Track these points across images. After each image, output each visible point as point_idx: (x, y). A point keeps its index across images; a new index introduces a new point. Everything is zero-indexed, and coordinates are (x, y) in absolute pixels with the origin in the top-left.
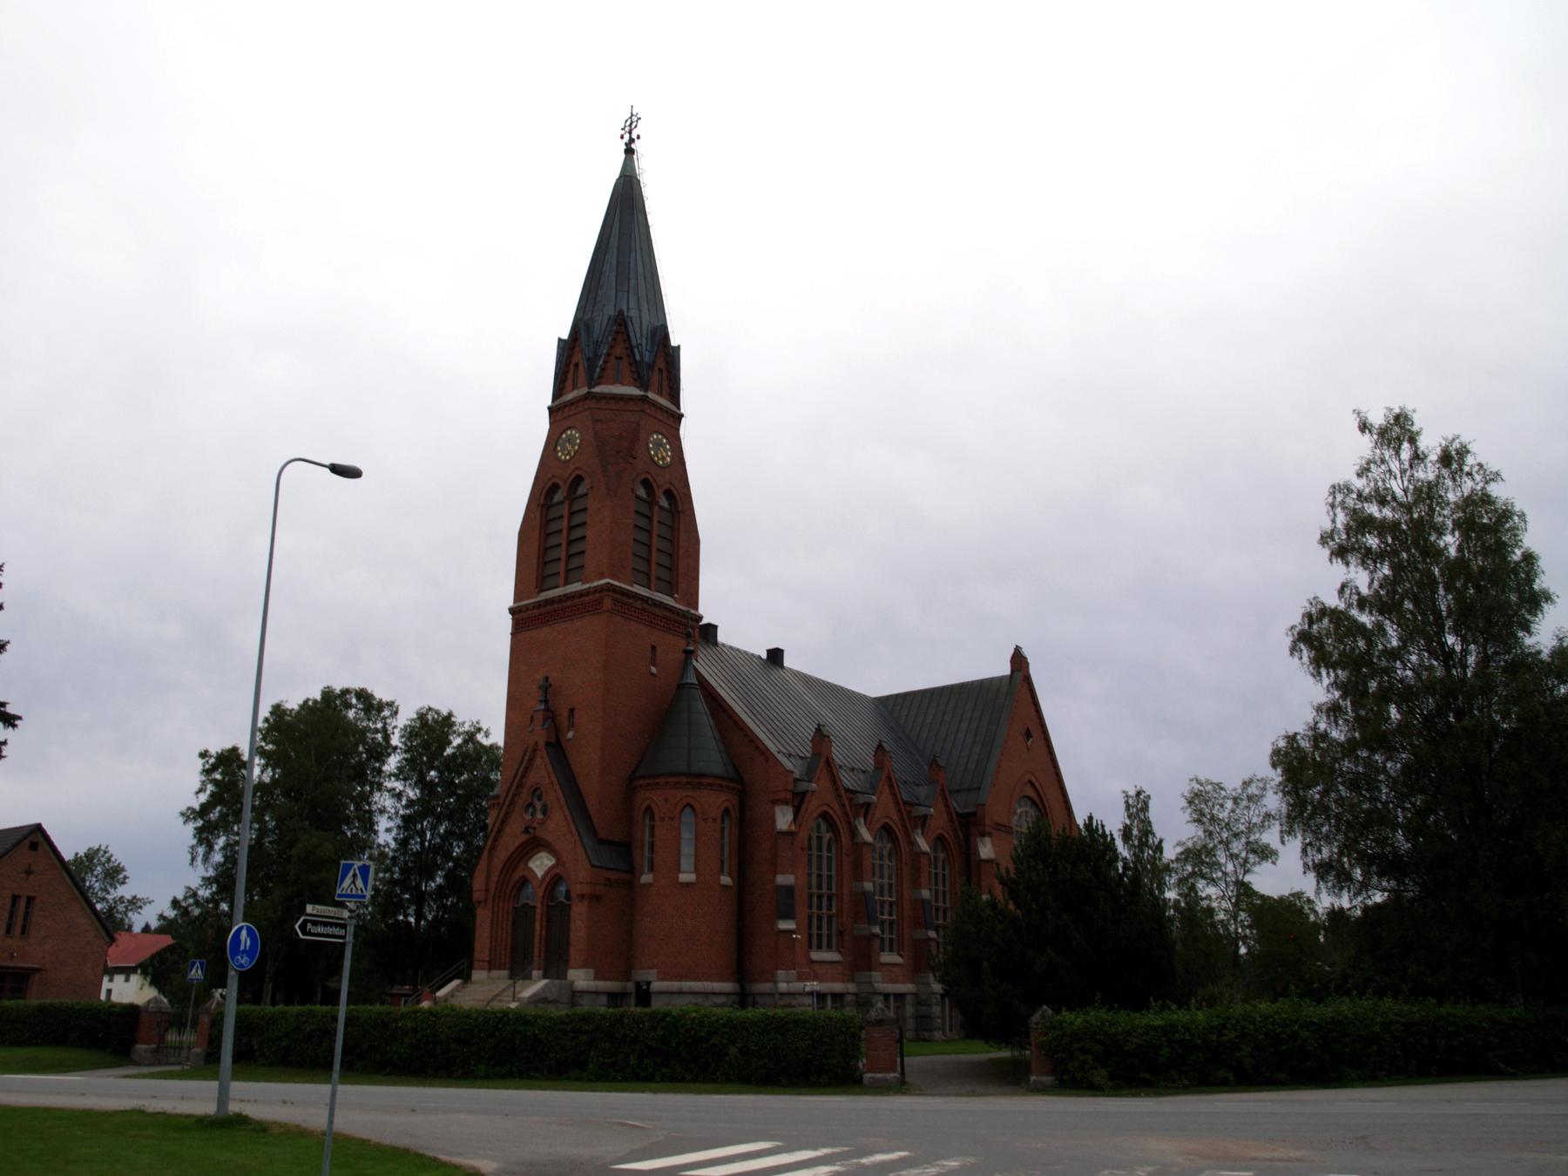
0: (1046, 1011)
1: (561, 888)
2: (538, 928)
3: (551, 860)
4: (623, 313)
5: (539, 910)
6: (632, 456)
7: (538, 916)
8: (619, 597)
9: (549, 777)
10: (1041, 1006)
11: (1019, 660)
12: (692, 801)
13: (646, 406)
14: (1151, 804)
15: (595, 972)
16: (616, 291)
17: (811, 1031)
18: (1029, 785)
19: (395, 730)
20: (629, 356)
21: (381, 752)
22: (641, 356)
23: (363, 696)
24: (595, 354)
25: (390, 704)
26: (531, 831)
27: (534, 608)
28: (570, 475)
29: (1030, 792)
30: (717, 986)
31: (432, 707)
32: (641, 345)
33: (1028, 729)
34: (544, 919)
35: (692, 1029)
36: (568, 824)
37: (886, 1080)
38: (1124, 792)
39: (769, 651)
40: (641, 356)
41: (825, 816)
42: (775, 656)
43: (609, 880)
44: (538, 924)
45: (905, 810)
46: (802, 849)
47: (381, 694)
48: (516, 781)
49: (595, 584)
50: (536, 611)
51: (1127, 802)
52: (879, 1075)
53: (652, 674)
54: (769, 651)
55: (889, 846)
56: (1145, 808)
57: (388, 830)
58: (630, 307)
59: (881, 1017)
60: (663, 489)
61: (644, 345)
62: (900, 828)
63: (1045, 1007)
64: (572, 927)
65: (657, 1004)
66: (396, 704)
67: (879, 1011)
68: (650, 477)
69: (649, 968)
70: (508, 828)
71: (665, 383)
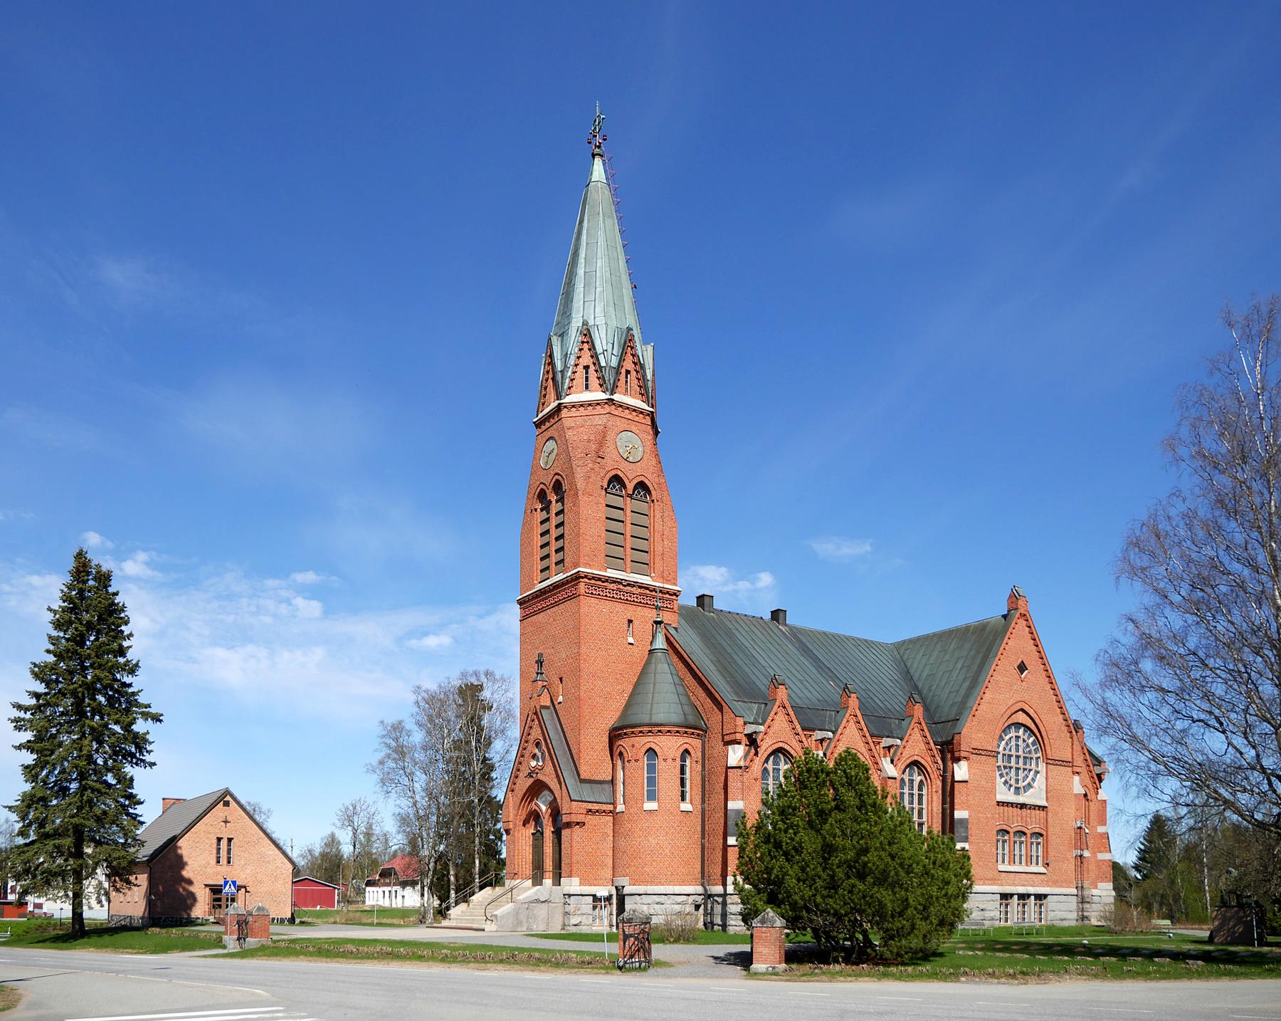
8: (593, 581)
11: (1014, 598)
12: (653, 746)
15: (580, 879)
20: (594, 364)
24: (566, 366)
26: (534, 775)
35: (830, 856)
42: (777, 615)
43: (590, 810)
45: (873, 742)
46: (756, 780)
49: (571, 573)
68: (619, 473)
69: (624, 876)
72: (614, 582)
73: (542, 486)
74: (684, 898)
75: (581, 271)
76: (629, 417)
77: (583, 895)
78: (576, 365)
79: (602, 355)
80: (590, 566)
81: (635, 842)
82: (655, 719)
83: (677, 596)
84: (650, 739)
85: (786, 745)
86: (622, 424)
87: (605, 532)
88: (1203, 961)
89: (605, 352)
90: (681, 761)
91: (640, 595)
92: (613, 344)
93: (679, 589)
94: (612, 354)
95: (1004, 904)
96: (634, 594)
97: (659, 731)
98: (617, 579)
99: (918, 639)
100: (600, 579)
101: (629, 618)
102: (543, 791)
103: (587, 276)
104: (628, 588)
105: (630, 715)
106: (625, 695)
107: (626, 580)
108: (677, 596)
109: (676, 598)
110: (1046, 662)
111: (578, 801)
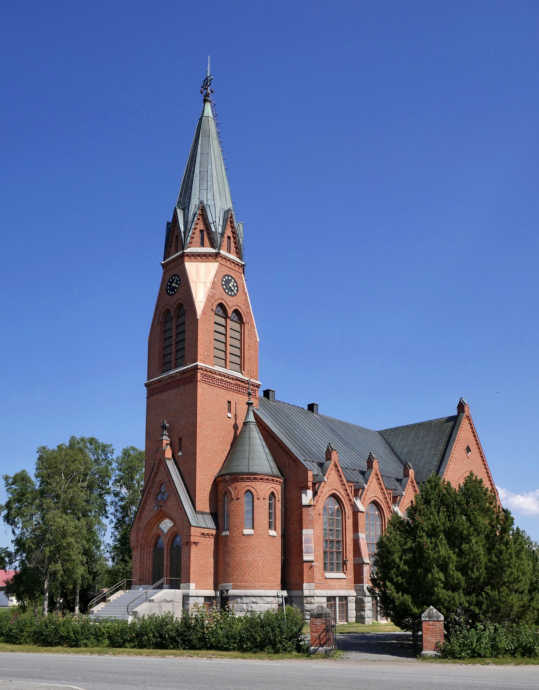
0: (432, 610)
1: (178, 539)
2: (165, 561)
7: (165, 555)
10: (429, 606)
11: (461, 407)
12: (251, 489)
16: (200, 190)
21: (104, 475)
22: (216, 229)
23: (92, 441)
30: (274, 592)
33: (468, 446)
34: (169, 556)
40: (216, 229)
41: (334, 496)
42: (311, 407)
43: (203, 534)
44: (165, 559)
45: (387, 493)
47: (102, 440)
48: (150, 480)
50: (159, 384)
58: (208, 199)
59: (320, 612)
61: (217, 222)
62: (384, 503)
63: (431, 607)
64: (182, 561)
66: (113, 447)
68: (223, 302)
70: (147, 507)
71: (233, 245)
73: (166, 307)
74: (272, 599)
76: (230, 266)
77: (197, 597)
78: (195, 229)
79: (213, 224)
80: (204, 362)
81: (237, 558)
83: (258, 388)
84: (248, 484)
85: (337, 492)
87: (213, 340)
89: (215, 223)
90: (269, 501)
91: (236, 385)
92: (219, 218)
93: (260, 383)
94: (219, 224)
95: (341, 616)
96: (231, 384)
99: (397, 429)
102: (165, 519)
103: (201, 174)
105: (233, 466)
108: (258, 388)
109: (258, 389)
110: (480, 447)
111: (195, 527)
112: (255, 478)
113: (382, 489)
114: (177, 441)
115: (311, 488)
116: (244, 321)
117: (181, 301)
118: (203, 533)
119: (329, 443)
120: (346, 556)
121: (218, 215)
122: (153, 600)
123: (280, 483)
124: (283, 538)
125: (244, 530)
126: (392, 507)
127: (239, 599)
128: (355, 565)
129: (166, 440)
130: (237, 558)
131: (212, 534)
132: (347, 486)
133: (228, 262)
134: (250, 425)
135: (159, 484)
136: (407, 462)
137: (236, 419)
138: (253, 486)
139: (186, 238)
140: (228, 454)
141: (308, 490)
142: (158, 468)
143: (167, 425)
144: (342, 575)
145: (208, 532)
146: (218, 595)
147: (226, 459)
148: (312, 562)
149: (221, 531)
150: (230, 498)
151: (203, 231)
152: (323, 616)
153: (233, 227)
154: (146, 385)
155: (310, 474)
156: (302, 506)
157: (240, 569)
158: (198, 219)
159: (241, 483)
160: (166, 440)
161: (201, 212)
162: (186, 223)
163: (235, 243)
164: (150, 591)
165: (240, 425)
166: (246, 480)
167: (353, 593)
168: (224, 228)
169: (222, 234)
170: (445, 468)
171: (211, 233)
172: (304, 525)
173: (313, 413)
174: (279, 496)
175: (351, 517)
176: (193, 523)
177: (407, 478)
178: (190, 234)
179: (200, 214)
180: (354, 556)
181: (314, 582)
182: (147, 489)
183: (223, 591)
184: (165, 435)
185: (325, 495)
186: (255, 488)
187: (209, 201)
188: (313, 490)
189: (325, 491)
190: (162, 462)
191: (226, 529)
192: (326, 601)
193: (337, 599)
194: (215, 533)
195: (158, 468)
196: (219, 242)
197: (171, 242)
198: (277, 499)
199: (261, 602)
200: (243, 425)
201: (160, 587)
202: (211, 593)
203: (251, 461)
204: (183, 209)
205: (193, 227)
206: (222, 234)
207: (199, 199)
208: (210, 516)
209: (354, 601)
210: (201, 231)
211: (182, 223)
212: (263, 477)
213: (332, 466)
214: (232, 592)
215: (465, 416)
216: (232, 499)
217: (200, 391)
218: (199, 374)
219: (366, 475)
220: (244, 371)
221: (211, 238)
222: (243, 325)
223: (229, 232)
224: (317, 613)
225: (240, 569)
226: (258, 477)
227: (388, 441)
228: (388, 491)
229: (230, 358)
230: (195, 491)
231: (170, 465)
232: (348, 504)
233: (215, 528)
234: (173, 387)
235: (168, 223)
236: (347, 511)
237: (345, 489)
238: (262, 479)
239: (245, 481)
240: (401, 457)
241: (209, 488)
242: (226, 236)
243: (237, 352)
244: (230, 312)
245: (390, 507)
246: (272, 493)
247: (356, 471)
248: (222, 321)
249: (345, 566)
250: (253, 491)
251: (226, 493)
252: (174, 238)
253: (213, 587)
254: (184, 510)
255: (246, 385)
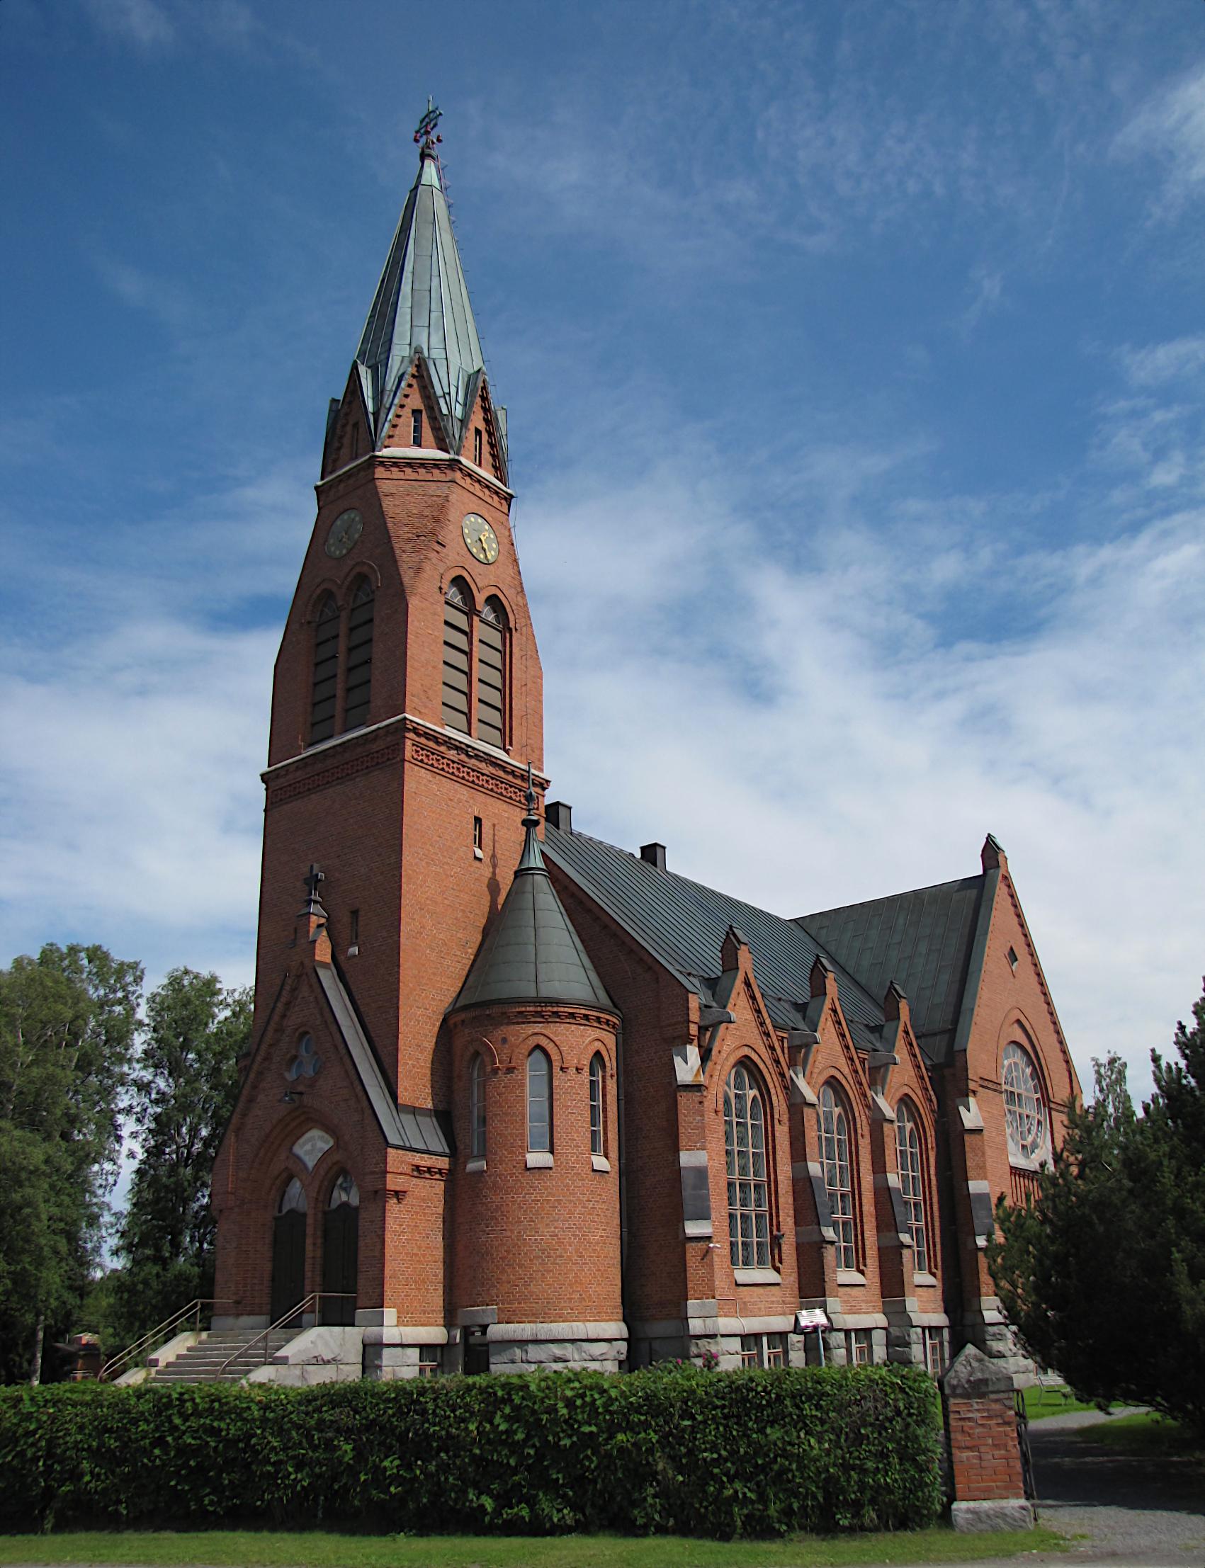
3: (327, 1142)
4: (422, 353)
5: (310, 1221)
6: (438, 543)
7: (309, 1230)
8: (423, 740)
9: (322, 1014)
11: (991, 852)
12: (544, 1042)
13: (458, 475)
14: (1128, 1073)
15: (398, 1312)
17: (832, 1414)
18: (1016, 1026)
19: (139, 1000)
21: (118, 1035)
22: (450, 410)
23: (97, 955)
25: (134, 966)
27: (297, 769)
28: (348, 575)
29: (1020, 1037)
31: (189, 968)
32: (449, 394)
34: (319, 1233)
36: (352, 1084)
37: (1002, 1515)
38: (1093, 1059)
39: (643, 849)
40: (450, 410)
42: (652, 853)
43: (417, 1168)
44: (309, 1241)
45: (859, 1058)
47: (119, 954)
50: (299, 773)
51: (1098, 1072)
52: (986, 1505)
53: (476, 858)
54: (643, 849)
55: (837, 1110)
56: (1121, 1078)
57: (134, 1135)
59: (979, 1375)
60: (486, 594)
62: (852, 1082)
64: (361, 1244)
65: (500, 1368)
66: (141, 966)
67: (975, 1364)
68: (465, 575)
71: (486, 449)
72: (457, 748)
75: (406, 288)
76: (480, 494)
78: (402, 406)
80: (421, 714)
82: (548, 990)
84: (538, 1028)
86: (474, 504)
88: (1069, 1381)
94: (457, 401)
97: (556, 1014)
98: (461, 742)
100: (436, 740)
101: (476, 814)
102: (310, 1129)
104: (473, 761)
106: (470, 951)
107: (474, 749)
108: (544, 789)
112: (556, 1014)
113: (847, 1047)
114: (346, 919)
115: (696, 1042)
116: (512, 625)
117: (365, 569)
118: (418, 1167)
119: (731, 926)
120: (778, 1223)
121: (453, 382)
122: (286, 1358)
123: (614, 1027)
124: (624, 1179)
125: (528, 1156)
126: (870, 1093)
127: (518, 1351)
128: (799, 1248)
129: (317, 916)
130: (508, 1233)
131: (440, 1169)
132: (774, 1038)
133: (477, 485)
134: (535, 877)
135: (297, 1034)
136: (892, 982)
137: (494, 866)
138: (551, 1036)
139: (380, 425)
140: (477, 956)
141: (688, 1047)
142: (294, 990)
143: (321, 875)
144: (769, 1276)
145: (429, 1164)
146: (458, 1340)
147: (472, 966)
148: (709, 1238)
149: (462, 1160)
150: (489, 1069)
151: (420, 411)
152: (991, 1388)
153: (486, 410)
154: (264, 777)
155: (694, 1003)
156: (675, 1089)
157: (520, 1266)
158: (410, 386)
159: (517, 1027)
160: (317, 916)
161: (417, 371)
162: (379, 393)
163: (492, 446)
164: (277, 1334)
165: (506, 879)
166: (533, 1020)
167: (879, 1319)
168: (467, 407)
169: (464, 422)
170: (974, 999)
171: (439, 417)
172: (683, 1141)
173: (655, 865)
174: (611, 1064)
175: (785, 1118)
176: (393, 1138)
177: (896, 1022)
178: (390, 417)
179: (413, 376)
180: (796, 1223)
181: (714, 1298)
182: (264, 1047)
183: (473, 1329)
184: (316, 902)
185: (726, 1059)
186: (555, 1039)
187: (432, 351)
188: (700, 1046)
189: (728, 1046)
190: (308, 973)
191: (475, 1153)
192: (739, 1348)
193: (765, 1339)
194: (447, 1167)
195: (296, 989)
196: (457, 437)
197: (341, 437)
198: (608, 1069)
199: (576, 1357)
200: (515, 878)
201: (297, 1325)
202: (435, 1334)
203: (542, 967)
204: (374, 369)
205: (396, 401)
206: (464, 422)
207: (410, 345)
208: (434, 1119)
209: (801, 1345)
210: (414, 412)
211: (370, 394)
212: (574, 1011)
213: (739, 984)
214: (497, 1331)
215: (1000, 877)
216: (496, 1071)
217: (410, 785)
218: (408, 743)
219: (809, 1013)
220: (511, 745)
221: (440, 429)
222: (508, 635)
223: (477, 420)
224: (969, 1381)
225: (520, 1266)
226: (562, 1009)
227: (821, 941)
228: (860, 1055)
229: (479, 711)
230: (397, 1050)
231: (328, 978)
232: (777, 1084)
233: (447, 1150)
234: (338, 778)
235: (334, 401)
236: (775, 1103)
237: (770, 1046)
238: (572, 1015)
239: (529, 1022)
240: (858, 978)
241: (430, 1044)
242: (472, 427)
243: (494, 697)
244: (480, 599)
245: (865, 1096)
246: (598, 1054)
247: (782, 1002)
248: (461, 620)
249: (776, 1251)
250: (550, 1048)
251: (477, 1054)
252: (349, 428)
253: (440, 1318)
254: (365, 1103)
255: (516, 781)
